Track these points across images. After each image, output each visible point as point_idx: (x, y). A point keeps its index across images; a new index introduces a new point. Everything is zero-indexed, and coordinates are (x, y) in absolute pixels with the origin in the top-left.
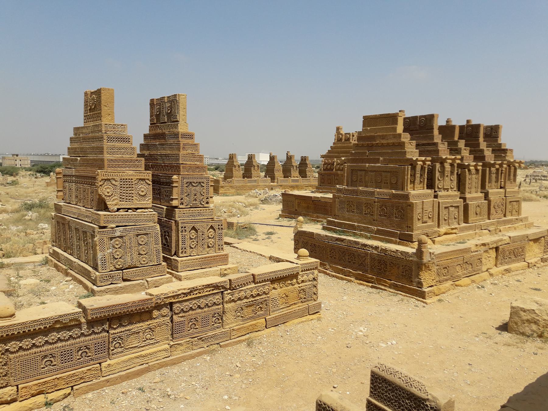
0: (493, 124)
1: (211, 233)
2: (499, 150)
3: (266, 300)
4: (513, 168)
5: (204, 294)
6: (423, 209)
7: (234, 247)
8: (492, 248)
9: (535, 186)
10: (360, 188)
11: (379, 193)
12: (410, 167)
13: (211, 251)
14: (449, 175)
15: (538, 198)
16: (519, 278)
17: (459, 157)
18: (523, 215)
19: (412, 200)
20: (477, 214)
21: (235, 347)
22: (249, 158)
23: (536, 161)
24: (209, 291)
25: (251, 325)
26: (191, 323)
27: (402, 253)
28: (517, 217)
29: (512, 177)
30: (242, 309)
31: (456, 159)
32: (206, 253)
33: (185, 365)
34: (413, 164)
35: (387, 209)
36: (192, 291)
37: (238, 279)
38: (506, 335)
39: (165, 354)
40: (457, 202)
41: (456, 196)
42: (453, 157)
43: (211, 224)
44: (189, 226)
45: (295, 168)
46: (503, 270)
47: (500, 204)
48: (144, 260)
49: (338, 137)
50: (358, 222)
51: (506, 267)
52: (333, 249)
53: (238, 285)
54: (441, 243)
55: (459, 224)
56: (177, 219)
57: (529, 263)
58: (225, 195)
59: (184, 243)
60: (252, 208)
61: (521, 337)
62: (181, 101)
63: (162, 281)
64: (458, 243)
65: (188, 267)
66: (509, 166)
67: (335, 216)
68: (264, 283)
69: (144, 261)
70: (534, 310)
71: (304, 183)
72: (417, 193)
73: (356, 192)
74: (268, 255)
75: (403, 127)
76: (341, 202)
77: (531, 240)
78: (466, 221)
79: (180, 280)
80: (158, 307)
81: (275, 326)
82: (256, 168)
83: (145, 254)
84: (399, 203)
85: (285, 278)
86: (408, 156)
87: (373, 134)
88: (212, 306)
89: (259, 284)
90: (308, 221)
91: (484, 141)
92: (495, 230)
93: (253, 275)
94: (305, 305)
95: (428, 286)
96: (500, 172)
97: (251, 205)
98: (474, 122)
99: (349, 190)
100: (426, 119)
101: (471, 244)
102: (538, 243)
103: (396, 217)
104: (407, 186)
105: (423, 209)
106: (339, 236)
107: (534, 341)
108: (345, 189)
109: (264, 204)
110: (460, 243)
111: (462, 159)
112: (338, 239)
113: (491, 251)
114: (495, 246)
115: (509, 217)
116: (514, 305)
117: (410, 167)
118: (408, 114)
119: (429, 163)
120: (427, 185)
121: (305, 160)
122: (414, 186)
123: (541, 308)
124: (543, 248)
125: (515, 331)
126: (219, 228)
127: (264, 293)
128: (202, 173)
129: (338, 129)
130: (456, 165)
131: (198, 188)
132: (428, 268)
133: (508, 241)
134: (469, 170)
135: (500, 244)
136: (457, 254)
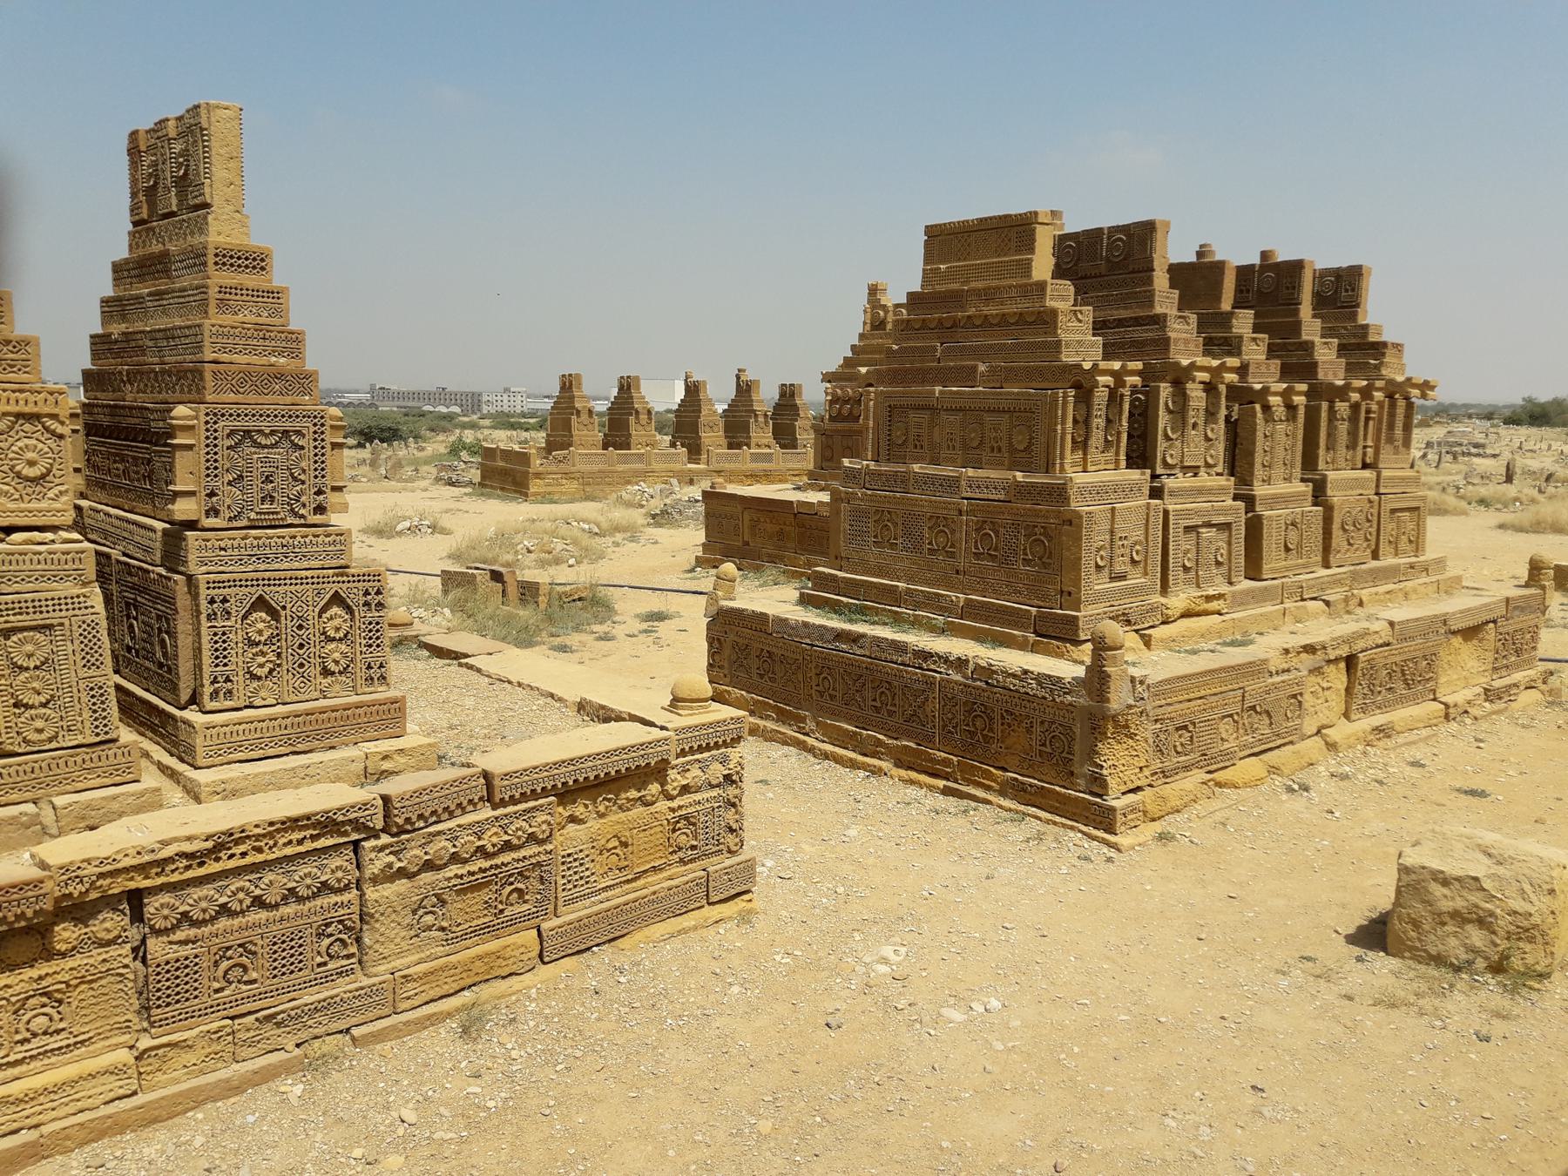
0: (1343, 261)
1: (336, 622)
2: (1359, 347)
3: (539, 864)
4: (1401, 403)
5: (278, 854)
6: (1112, 532)
7: (470, 667)
8: (1337, 660)
9: (1453, 472)
10: (916, 467)
11: (971, 482)
12: (1072, 392)
13: (337, 687)
14: (1201, 422)
15: (1464, 504)
16: (1417, 753)
17: (1233, 362)
18: (1430, 554)
19: (1076, 504)
20: (1287, 549)
21: (410, 1041)
22: (621, 388)
23: (1453, 406)
24: (300, 842)
25: (480, 957)
26: (225, 965)
27: (1041, 679)
28: (1414, 559)
29: (1399, 432)
30: (443, 902)
31: (1223, 367)
32: (316, 694)
33: (197, 1127)
34: (1083, 386)
35: (997, 533)
36: (221, 844)
37: (419, 792)
38: (1382, 964)
39: (114, 1086)
40: (1224, 511)
41: (1222, 490)
42: (1215, 363)
43: (335, 587)
44: (240, 597)
45: (761, 419)
46: (1369, 729)
47: (1362, 517)
48: (36, 726)
49: (874, 316)
50: (910, 580)
51: (1379, 719)
52: (826, 666)
53: (421, 817)
54: (1170, 644)
55: (1231, 583)
56: (193, 568)
57: (1447, 706)
58: (547, 498)
59: (220, 657)
60: (619, 537)
61: (1432, 971)
62: (218, 128)
63: (115, 806)
64: (1225, 644)
65: (239, 747)
66: (1390, 396)
67: (838, 561)
68: (532, 804)
69: (40, 731)
70: (1476, 879)
71: (791, 465)
72: (1095, 479)
73: (902, 481)
74: (573, 696)
75: (1053, 261)
76: (858, 515)
77: (1454, 633)
78: (1254, 570)
79: (198, 800)
80: (78, 910)
81: (578, 952)
82: (643, 417)
83: (44, 705)
84: (1037, 514)
85: (614, 780)
86: (1068, 357)
87: (955, 286)
88: (315, 896)
89: (511, 809)
90: (782, 578)
91: (1314, 316)
92: (1346, 600)
93: (486, 775)
94: (694, 871)
95: (1124, 788)
96: (1363, 415)
97: (617, 529)
98: (1283, 255)
99: (880, 474)
100: (1129, 236)
101: (1267, 647)
102: (1475, 642)
103: (1027, 562)
104: (1062, 457)
105: (1112, 532)
106: (847, 626)
107: (1474, 986)
108: (869, 473)
109: (660, 526)
110: (1233, 644)
111: (1243, 370)
112: (840, 636)
113: (1330, 670)
114: (1344, 651)
115: (1388, 561)
116: (1408, 861)
117: (1072, 392)
118: (1075, 223)
119: (1136, 380)
120: (1129, 458)
121: (792, 395)
122: (1085, 460)
123: (1501, 870)
124: (1490, 656)
125: (1411, 949)
126: (366, 604)
127: (532, 838)
128: (298, 399)
129: (873, 290)
130: (1222, 388)
131: (277, 455)
132: (1124, 730)
133: (1386, 635)
134: (1267, 408)
135: (1361, 644)
136: (1223, 682)
